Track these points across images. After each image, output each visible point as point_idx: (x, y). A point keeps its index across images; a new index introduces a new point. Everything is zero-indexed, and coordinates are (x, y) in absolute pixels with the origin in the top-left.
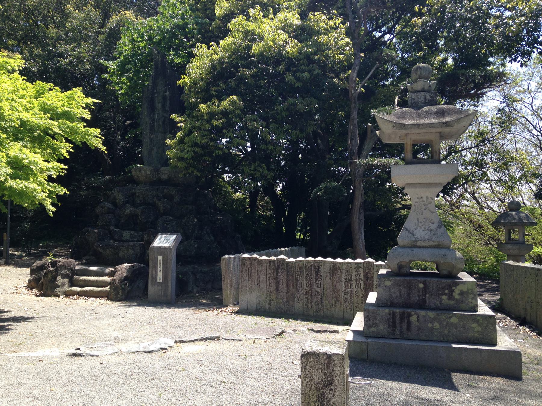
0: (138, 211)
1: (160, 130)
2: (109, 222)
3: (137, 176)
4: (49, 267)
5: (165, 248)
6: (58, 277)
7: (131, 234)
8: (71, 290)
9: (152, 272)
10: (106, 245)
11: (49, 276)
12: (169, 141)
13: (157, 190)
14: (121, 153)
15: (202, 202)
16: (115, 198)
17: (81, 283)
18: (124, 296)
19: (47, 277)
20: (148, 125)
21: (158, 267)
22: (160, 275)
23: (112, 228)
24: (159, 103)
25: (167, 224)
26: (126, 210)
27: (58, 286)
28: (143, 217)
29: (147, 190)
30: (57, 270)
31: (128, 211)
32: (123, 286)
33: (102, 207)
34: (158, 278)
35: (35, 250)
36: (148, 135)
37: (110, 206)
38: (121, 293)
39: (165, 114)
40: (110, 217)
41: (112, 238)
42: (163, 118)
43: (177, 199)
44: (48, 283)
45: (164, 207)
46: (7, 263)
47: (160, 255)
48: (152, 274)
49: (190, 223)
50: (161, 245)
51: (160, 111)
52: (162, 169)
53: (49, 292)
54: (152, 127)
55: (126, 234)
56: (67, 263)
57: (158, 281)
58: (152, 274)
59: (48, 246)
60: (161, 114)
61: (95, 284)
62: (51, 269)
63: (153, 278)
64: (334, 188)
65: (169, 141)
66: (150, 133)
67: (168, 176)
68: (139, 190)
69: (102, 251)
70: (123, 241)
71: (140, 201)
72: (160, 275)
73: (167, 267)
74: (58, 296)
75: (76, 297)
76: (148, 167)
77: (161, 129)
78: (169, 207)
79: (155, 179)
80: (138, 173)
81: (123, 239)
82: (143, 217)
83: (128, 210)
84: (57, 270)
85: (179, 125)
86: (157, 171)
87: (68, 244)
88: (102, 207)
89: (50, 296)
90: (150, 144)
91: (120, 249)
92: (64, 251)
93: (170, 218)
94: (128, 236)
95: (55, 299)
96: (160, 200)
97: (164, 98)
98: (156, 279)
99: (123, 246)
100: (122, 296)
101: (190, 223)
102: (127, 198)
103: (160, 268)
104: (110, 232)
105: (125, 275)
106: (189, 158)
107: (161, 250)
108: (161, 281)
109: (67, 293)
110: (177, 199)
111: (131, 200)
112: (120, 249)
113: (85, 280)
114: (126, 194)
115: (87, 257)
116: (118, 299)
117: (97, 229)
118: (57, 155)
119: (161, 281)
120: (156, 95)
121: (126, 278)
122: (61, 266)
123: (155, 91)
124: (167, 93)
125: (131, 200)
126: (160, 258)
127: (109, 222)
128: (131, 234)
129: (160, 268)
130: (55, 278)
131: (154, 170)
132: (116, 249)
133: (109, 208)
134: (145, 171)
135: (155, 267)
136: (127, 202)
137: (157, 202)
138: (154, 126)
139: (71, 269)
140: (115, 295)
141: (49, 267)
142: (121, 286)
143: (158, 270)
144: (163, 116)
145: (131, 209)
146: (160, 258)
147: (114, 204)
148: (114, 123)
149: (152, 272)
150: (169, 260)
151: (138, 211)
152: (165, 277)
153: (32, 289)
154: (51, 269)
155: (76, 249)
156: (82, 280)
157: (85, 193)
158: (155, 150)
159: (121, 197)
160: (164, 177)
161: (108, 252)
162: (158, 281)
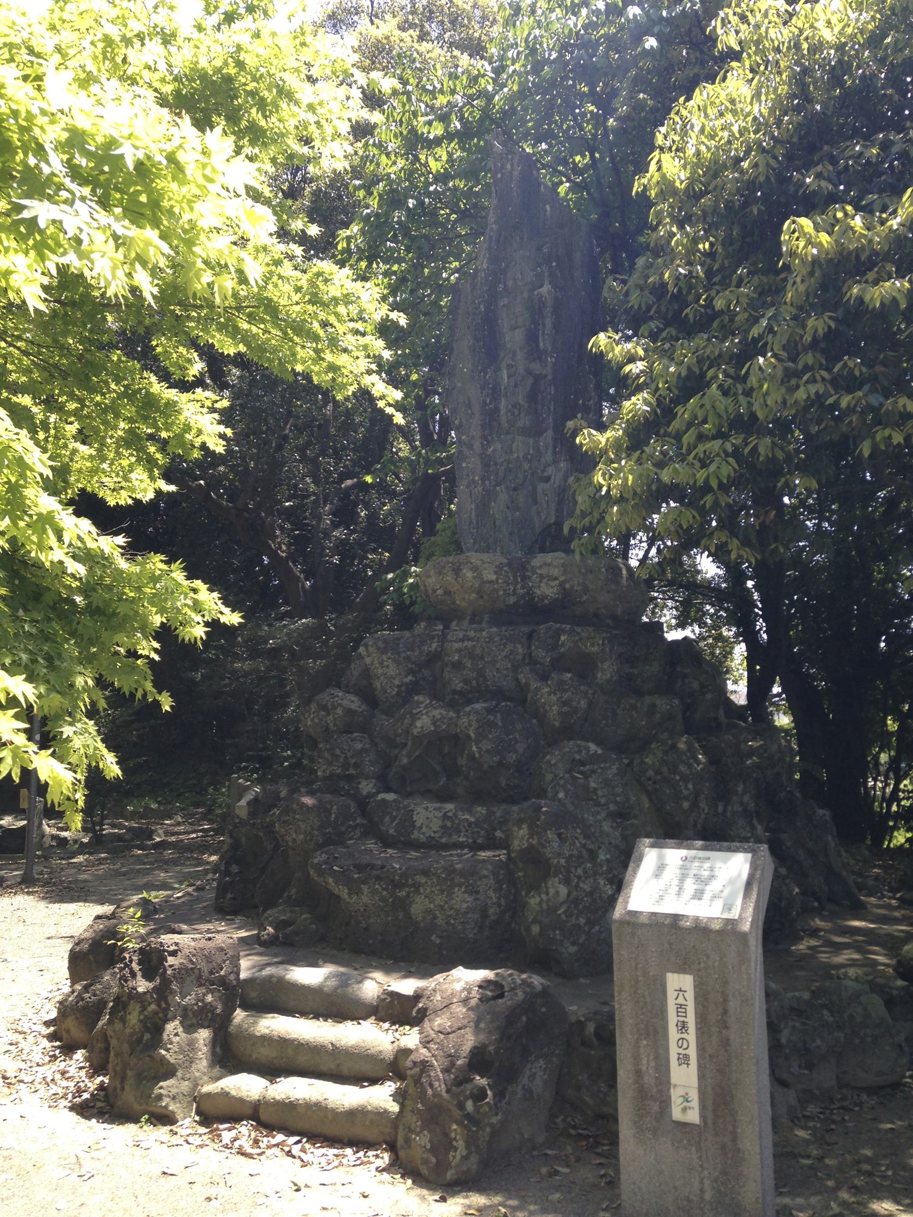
0: (468, 721)
1: (520, 424)
2: (356, 766)
3: (447, 593)
4: (133, 975)
5: (701, 929)
6: (170, 1027)
7: (445, 817)
8: (224, 1094)
9: (637, 1058)
10: (360, 868)
11: (134, 1017)
12: (590, 438)
13: (530, 636)
14: (336, 560)
15: (696, 685)
16: (367, 673)
17: (265, 1053)
18: (474, 1159)
19: (123, 1020)
20: (476, 409)
21: (673, 1034)
22: (684, 1080)
23: (366, 787)
24: (513, 328)
25: (586, 776)
26: (415, 717)
27: (169, 1072)
28: (486, 745)
29: (491, 639)
30: (162, 992)
31: (423, 723)
32: (469, 1105)
33: (324, 708)
34: (676, 1096)
35: (113, 826)
36: (477, 445)
37: (353, 702)
38: (460, 1144)
39: (536, 367)
40: (359, 746)
41: (372, 830)
42: (531, 380)
43: (606, 672)
44: (126, 1047)
45: (564, 704)
46: (27, 883)
47: (682, 969)
48: (638, 1073)
49: (683, 768)
50: (669, 907)
51: (520, 355)
52: (539, 560)
53: (129, 1097)
54: (491, 416)
55: (427, 816)
56: (208, 958)
57: (677, 1114)
58: (638, 1073)
59: (147, 813)
60: (521, 369)
61: (327, 1065)
62: (142, 985)
63: (642, 1093)
64: (751, 660)
65: (590, 438)
66: (484, 437)
67: (561, 585)
68: (459, 640)
69: (343, 892)
70: (417, 845)
71: (466, 681)
72: (684, 1080)
73: (725, 1043)
74: (164, 1119)
75: (245, 1129)
76: (485, 557)
77: (524, 421)
78: (583, 704)
79: (512, 600)
80: (450, 578)
81: (415, 835)
82: (486, 745)
83: (426, 718)
84: (162, 992)
85: (627, 369)
86: (520, 569)
87: (197, 805)
88: (324, 708)
89: (136, 1121)
90: (483, 479)
91: (417, 887)
92: (189, 828)
93: (593, 747)
94: (436, 825)
95: (152, 1135)
96: (544, 678)
97: (536, 309)
98: (665, 1103)
99: (426, 873)
100: (465, 1158)
101: (683, 768)
102: (411, 672)
103: (682, 1042)
104: (363, 804)
105: (469, 1041)
106: (714, 484)
107: (678, 939)
108: (693, 1117)
109: (207, 1107)
110: (606, 672)
111: (427, 678)
112: (417, 887)
113: (284, 1043)
114: (408, 658)
115: (278, 913)
116: (450, 1175)
117: (311, 793)
118: (164, 445)
119: (693, 1117)
120: (503, 302)
121: (479, 1060)
122: (183, 973)
123: (501, 287)
124: (546, 289)
125: (427, 678)
126: (680, 987)
127: (356, 766)
128: (445, 817)
129: (682, 1042)
130: (154, 1030)
131: (509, 565)
132: (398, 886)
133: (350, 712)
134: (475, 569)
135: (654, 1029)
136: (413, 689)
137: (534, 685)
138: (497, 410)
139: (223, 982)
140: (433, 1150)
141: (133, 975)
142: (461, 1106)
143: (674, 1051)
144: (529, 372)
145: (437, 713)
146: (680, 987)
147: (367, 694)
148: (316, 482)
149: (637, 1058)
150: (733, 1004)
151: (468, 721)
152: (718, 1095)
153: (68, 1050)
154: (142, 985)
155: (235, 869)
156: (267, 1039)
157: (247, 666)
158: (503, 497)
159: (392, 670)
160: (547, 591)
161: (363, 900)
162: (677, 1114)
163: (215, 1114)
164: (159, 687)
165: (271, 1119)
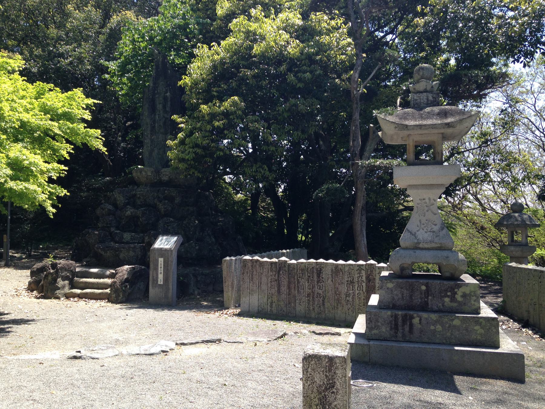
0: (139, 212)
1: (161, 131)
2: (110, 224)
3: (138, 178)
4: (49, 269)
5: (166, 250)
6: (59, 279)
7: (132, 236)
8: (72, 292)
9: (153, 274)
10: (107, 247)
11: (50, 278)
12: (170, 143)
13: (158, 191)
14: (122, 155)
15: (204, 204)
16: (115, 199)
17: (82, 285)
18: (124, 298)
19: (47, 279)
20: (149, 126)
21: (159, 269)
22: (161, 277)
23: (112, 229)
24: (160, 104)
25: (168, 226)
26: (126, 211)
27: (59, 289)
28: (144, 219)
29: (148, 191)
30: (57, 272)
31: (128, 213)
32: (124, 288)
33: (102, 209)
34: (159, 280)
35: (35, 252)
36: (149, 136)
37: (110, 207)
38: (121, 296)
39: (166, 115)
40: (110, 219)
41: (113, 240)
42: (164, 119)
43: (178, 200)
44: (48, 285)
45: (165, 208)
46: (7, 265)
47: (161, 257)
48: (153, 276)
49: (191, 224)
50: (161, 246)
51: (161, 112)
52: (163, 170)
53: (49, 294)
54: (153, 128)
55: (127, 236)
56: (68, 265)
57: (159, 283)
58: (153, 276)
59: (48, 248)
60: (162, 115)
61: (95, 286)
62: (52, 271)
63: (153, 280)
65: (170, 143)
66: (151, 134)
67: (169, 177)
68: (139, 191)
69: (103, 253)
70: (123, 243)
71: (141, 202)
72: (161, 277)
73: (168, 269)
74: (58, 298)
75: (76, 299)
76: (149, 169)
77: (162, 130)
78: (170, 208)
79: (156, 181)
80: (139, 174)
81: (124, 240)
82: (144, 219)
83: (129, 212)
84: (57, 272)
85: (180, 126)
86: (157, 172)
87: (68, 245)
88: (102, 209)
89: (51, 298)
90: (151, 146)
91: (121, 251)
92: (64, 253)
93: (171, 219)
94: (129, 238)
95: (55, 301)
96: (161, 202)
97: (165, 98)
98: (157, 281)
99: (124, 248)
100: (122, 298)
101: (191, 224)
102: (127, 199)
103: (161, 270)
104: (111, 234)
105: (126, 277)
106: (190, 159)
107: (162, 252)
108: (162, 283)
109: (67, 295)
110: (178, 200)
111: (131, 201)
112: (121, 251)
113: (86, 283)
114: (126, 196)
115: (88, 259)
116: (119, 301)
117: (97, 231)
118: (57, 156)
119: (162, 283)
120: (157, 96)
121: (127, 280)
122: (62, 268)
123: (156, 92)
124: (168, 94)
125: (131, 201)
126: (161, 260)
127: (110, 224)
128: (132, 236)
129: (161, 270)
130: (55, 280)
131: (155, 171)
132: (117, 251)
133: (109, 210)
134: (145, 172)
135: (156, 269)
136: (128, 204)
137: (158, 204)
138: (154, 126)
139: (72, 271)
140: (116, 297)
141: (49, 269)
142: (122, 288)
143: (159, 272)
144: (164, 117)
145: (132, 210)
146: (161, 260)
147: (115, 205)
148: (115, 124)
149: (153, 274)
150: (170, 262)
151: (139, 212)
152: (166, 279)
153: (32, 291)
154: (52, 271)
155: (76, 251)
156: (82, 282)
157: (86, 194)
158: (156, 151)
159: (122, 199)
160: (165, 178)
161: (108, 254)
162: (159, 283)
163: (68, 296)
164: (58, 203)
165: (80, 296)
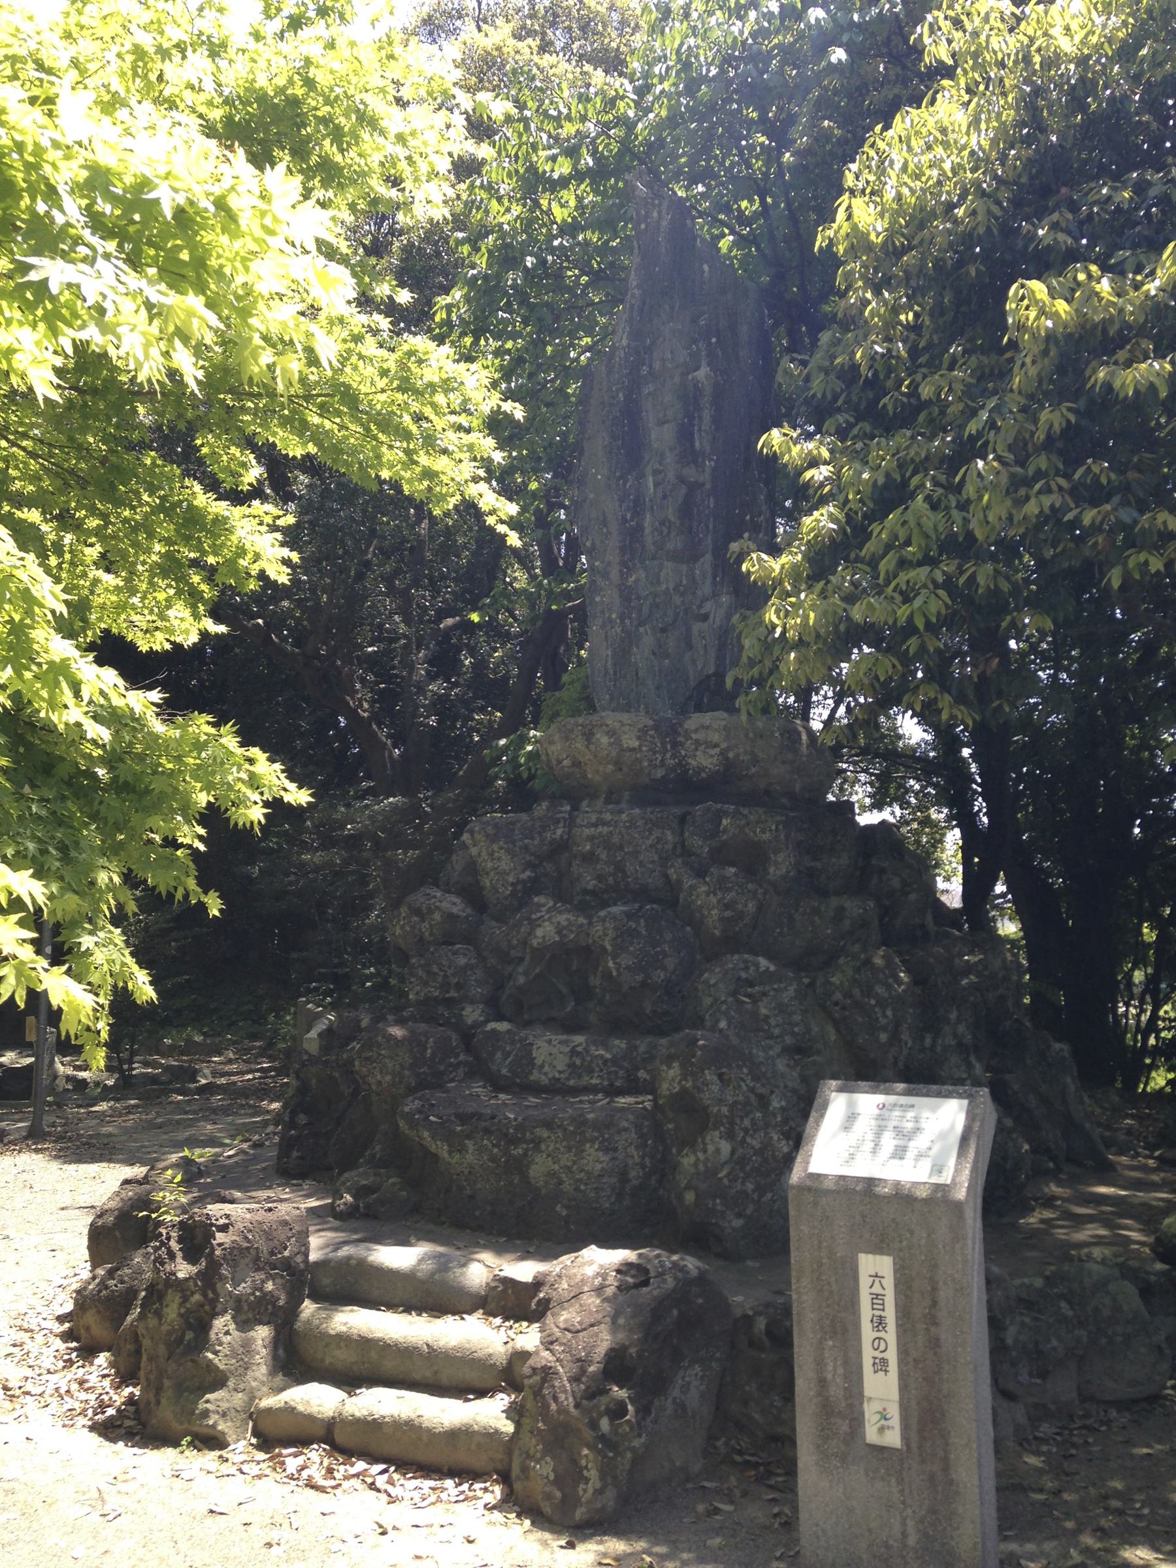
0: (602, 929)
1: (670, 546)
2: (459, 986)
3: (576, 764)
4: (172, 1256)
5: (903, 1197)
6: (219, 1323)
7: (573, 1052)
8: (289, 1410)
9: (820, 1363)
10: (463, 1118)
11: (172, 1311)
12: (759, 565)
13: (682, 820)
14: (432, 721)
15: (896, 883)
16: (472, 868)
17: (341, 1357)
18: (611, 1493)
19: (159, 1314)
20: (614, 527)
21: (867, 1333)
22: (882, 1392)
23: (472, 1014)
24: (661, 423)
25: (755, 999)
26: (534, 924)
27: (218, 1381)
28: (626, 960)
29: (632, 823)
30: (209, 1278)
31: (545, 932)
32: (605, 1424)
33: (417, 912)
34: (870, 1412)
35: (146, 1064)
36: (614, 574)
37: (454, 905)
38: (593, 1474)
39: (690, 473)
40: (462, 961)
41: (479, 1070)
42: (683, 490)
43: (781, 865)
44: (162, 1350)
45: (727, 907)
46: (34, 1138)
47: (878, 1249)
48: (822, 1383)
49: (879, 990)
50: (862, 1168)
51: (670, 458)
52: (694, 721)
53: (166, 1413)
54: (632, 536)
55: (550, 1052)
56: (268, 1235)
57: (871, 1435)
58: (822, 1383)
59: (190, 1048)
60: (671, 476)
61: (422, 1372)
62: (183, 1270)
63: (827, 1409)
64: (967, 850)
65: (759, 565)
66: (624, 564)
67: (723, 753)
68: (592, 825)
69: (442, 1149)
70: (537, 1089)
71: (600, 878)
72: (882, 1392)
73: (934, 1344)
74: (212, 1441)
75: (315, 1454)
76: (625, 717)
77: (675, 543)
78: (751, 906)
79: (659, 773)
80: (580, 745)
81: (535, 1076)
82: (626, 960)
83: (549, 925)
84: (209, 1278)
85: (808, 475)
86: (670, 733)
87: (254, 1037)
88: (417, 912)
89: (175, 1444)
90: (622, 617)
91: (537, 1142)
92: (243, 1067)
93: (763, 962)
94: (561, 1063)
95: (196, 1462)
96: (701, 873)
97: (690, 398)
98: (857, 1422)
99: (548, 1125)
100: (599, 1492)
101: (879, 990)
102: (529, 865)
103: (879, 1343)
104: (467, 1036)
105: (604, 1341)
106: (920, 624)
107: (874, 1210)
108: (893, 1439)
109: (267, 1426)
110: (781, 865)
111: (550, 873)
112: (537, 1142)
113: (366, 1344)
114: (526, 848)
115: (359, 1176)
116: (580, 1514)
117: (401, 1022)
118: (211, 574)
119: (893, 1439)
120: (648, 389)
121: (617, 1366)
122: (236, 1254)
123: (645, 370)
124: (703, 373)
125: (550, 873)
126: (876, 1271)
127: (459, 986)
128: (573, 1052)
129: (879, 1343)
130: (198, 1327)
131: (656, 728)
132: (513, 1141)
133: (450, 917)
134: (611, 733)
135: (842, 1326)
136: (532, 887)
137: (688, 882)
138: (640, 528)
139: (287, 1265)
140: (558, 1482)
141: (172, 1256)
142: (594, 1425)
143: (868, 1355)
144: (682, 480)
145: (562, 919)
146: (876, 1271)
147: (473, 895)
148: (407, 621)
149: (820, 1363)
150: (944, 1294)
151: (602, 929)
152: (925, 1411)
153: (88, 1352)
154: (183, 1270)
155: (302, 1119)
156: (343, 1339)
157: (318, 858)
158: (648, 640)
159: (506, 864)
160: (705, 761)
161: (467, 1159)
162: (871, 1435)
164: (205, 885)
